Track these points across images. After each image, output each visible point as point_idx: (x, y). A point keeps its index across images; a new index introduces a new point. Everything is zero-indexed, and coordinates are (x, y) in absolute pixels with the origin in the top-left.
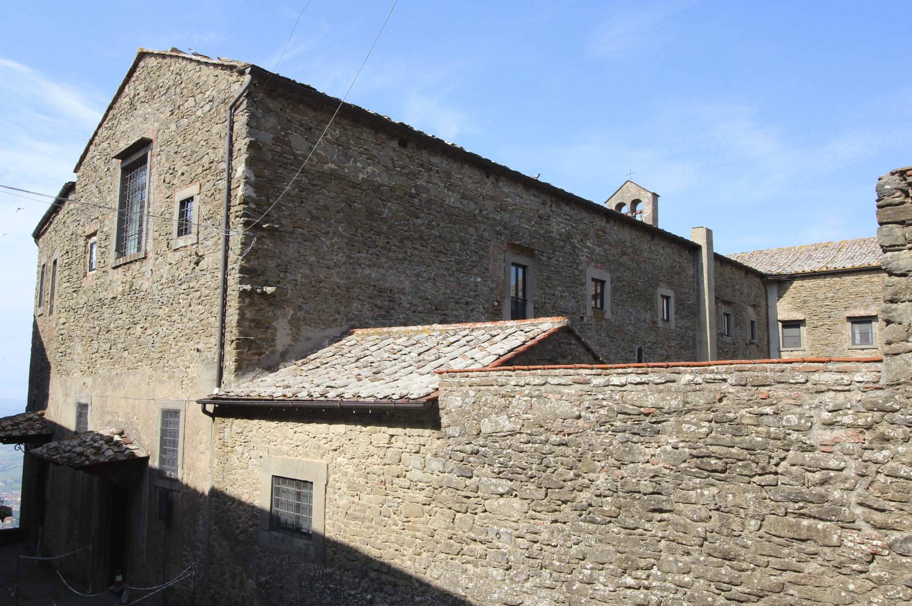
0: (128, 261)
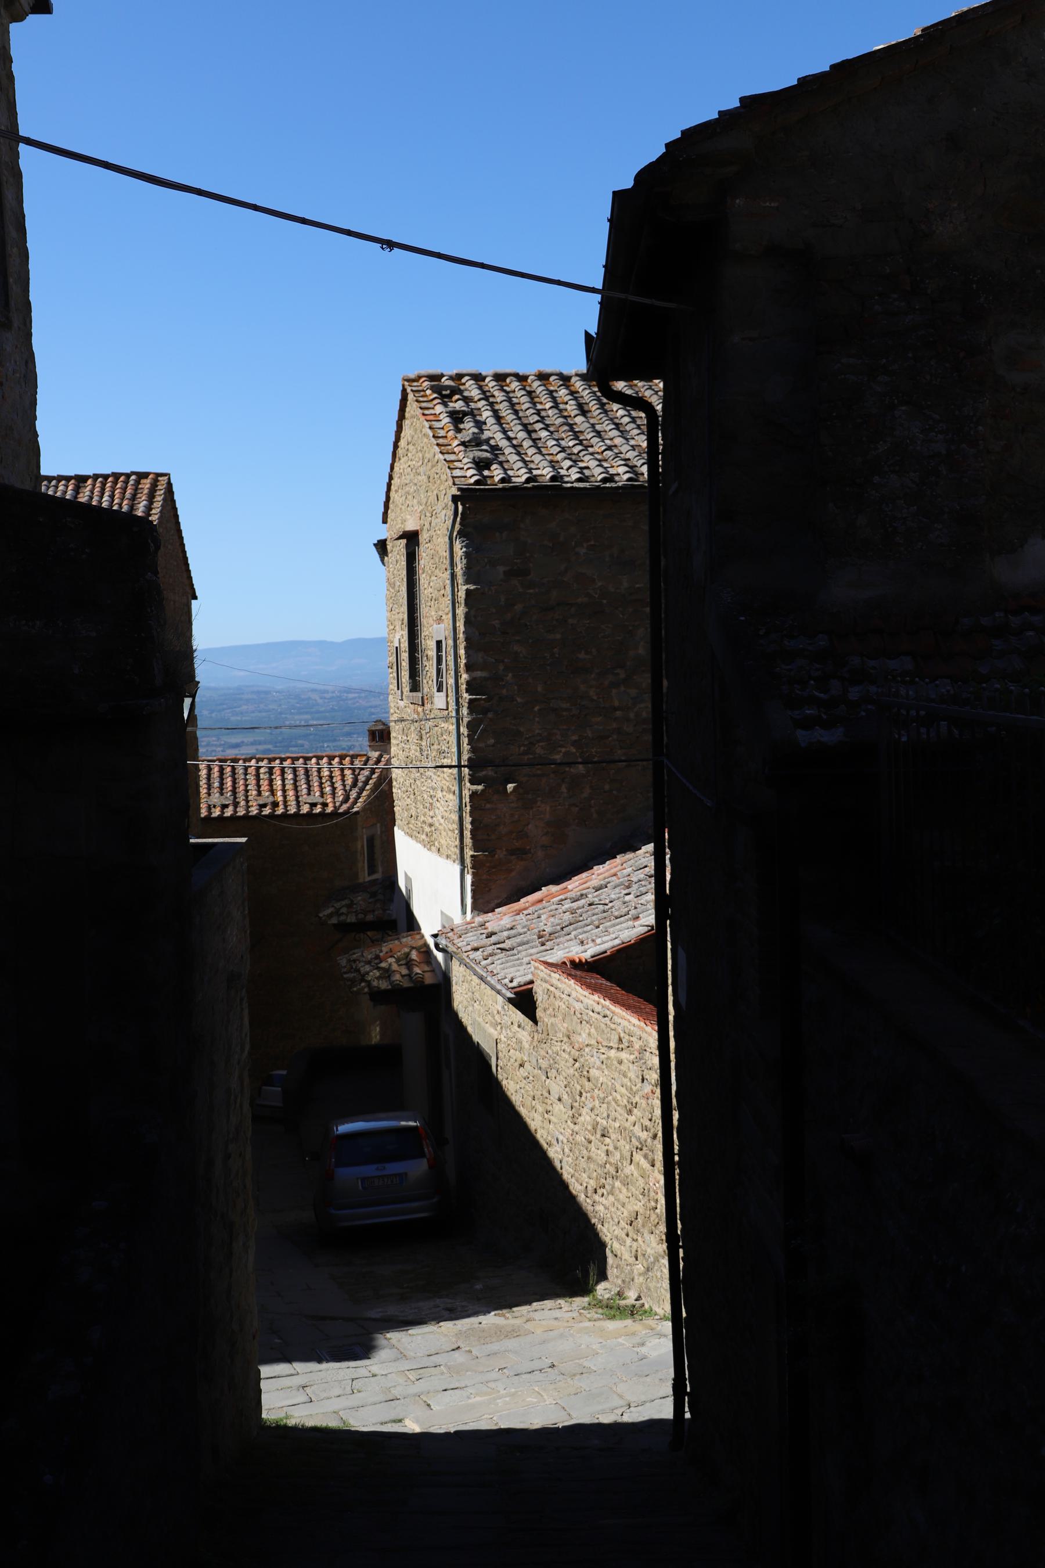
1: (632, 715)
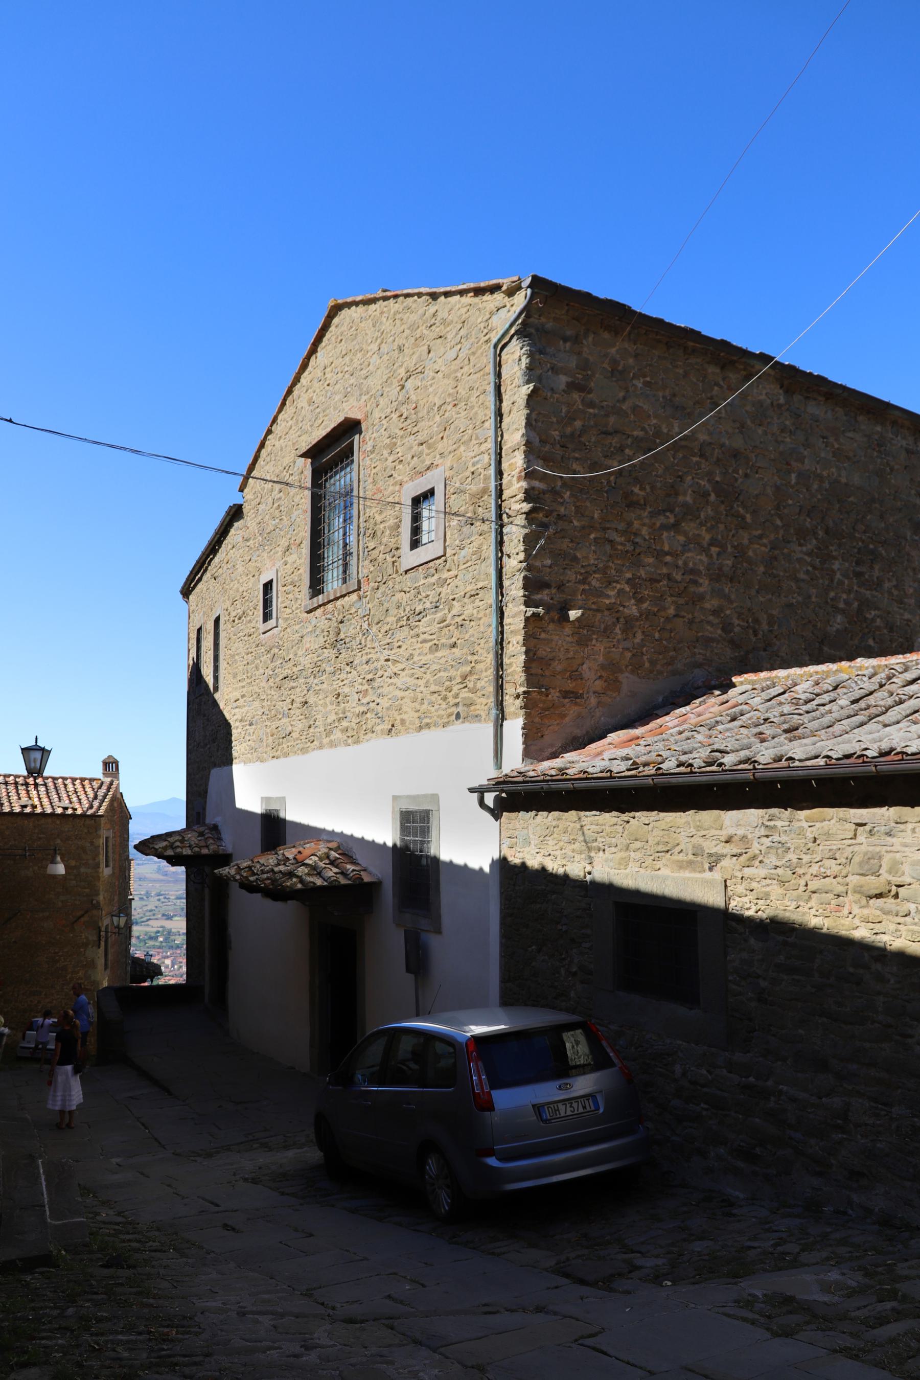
0: (332, 598)
1: (680, 563)
